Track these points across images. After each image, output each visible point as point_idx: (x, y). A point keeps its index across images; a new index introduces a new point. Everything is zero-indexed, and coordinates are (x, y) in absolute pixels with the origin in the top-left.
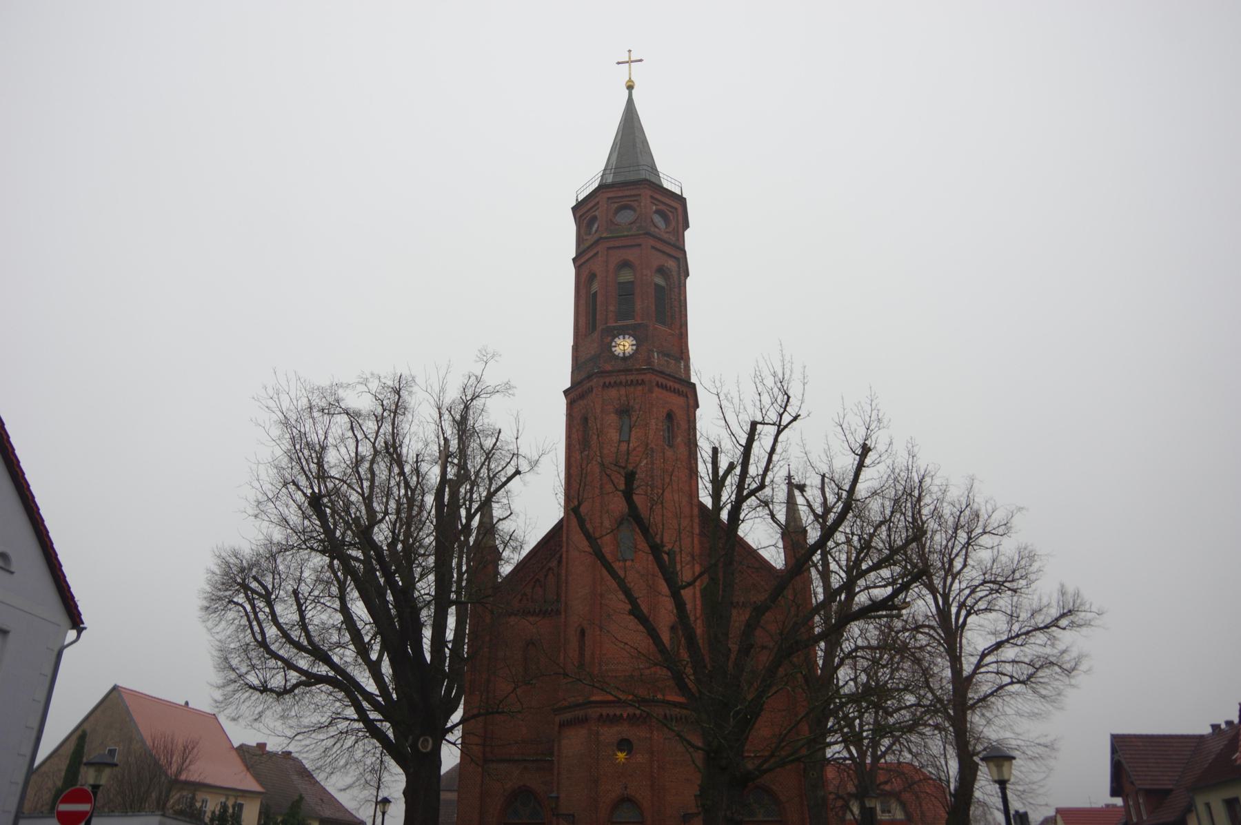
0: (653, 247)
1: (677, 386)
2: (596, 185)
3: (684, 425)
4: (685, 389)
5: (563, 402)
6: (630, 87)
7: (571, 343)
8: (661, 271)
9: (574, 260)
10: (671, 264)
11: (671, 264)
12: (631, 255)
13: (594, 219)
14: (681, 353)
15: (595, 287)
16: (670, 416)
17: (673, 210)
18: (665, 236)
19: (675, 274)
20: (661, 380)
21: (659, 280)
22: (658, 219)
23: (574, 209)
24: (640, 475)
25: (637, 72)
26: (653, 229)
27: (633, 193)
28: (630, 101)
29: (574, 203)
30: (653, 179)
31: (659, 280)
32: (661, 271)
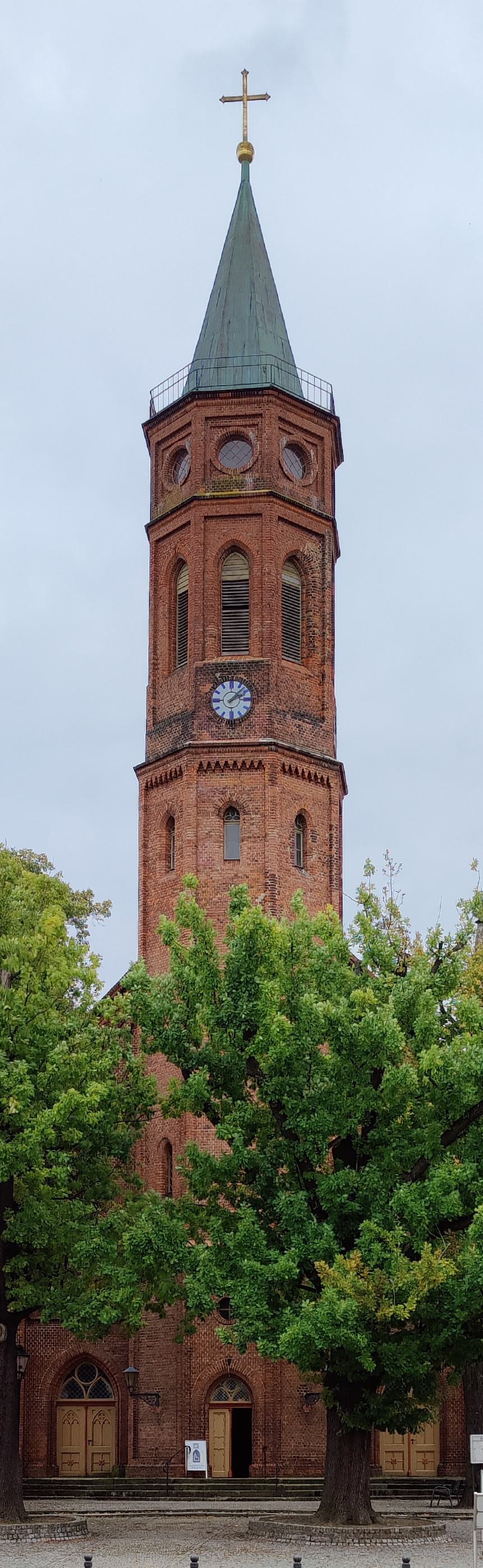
0: (280, 519)
1: (313, 769)
2: (175, 394)
3: (323, 834)
4: (322, 773)
5: (133, 785)
6: (246, 159)
7: (145, 682)
8: (293, 559)
9: (148, 527)
10: (310, 547)
11: (310, 547)
12: (245, 532)
13: (181, 452)
14: (321, 715)
15: (184, 583)
16: (301, 819)
17: (317, 435)
18: (301, 496)
19: (316, 564)
20: (287, 761)
21: (292, 579)
22: (292, 464)
23: (149, 427)
24: (258, 1419)
25: (264, 124)
26: (284, 483)
27: (249, 410)
28: (245, 192)
29: (147, 418)
30: (289, 387)
31: (292, 579)
32: (293, 559)
